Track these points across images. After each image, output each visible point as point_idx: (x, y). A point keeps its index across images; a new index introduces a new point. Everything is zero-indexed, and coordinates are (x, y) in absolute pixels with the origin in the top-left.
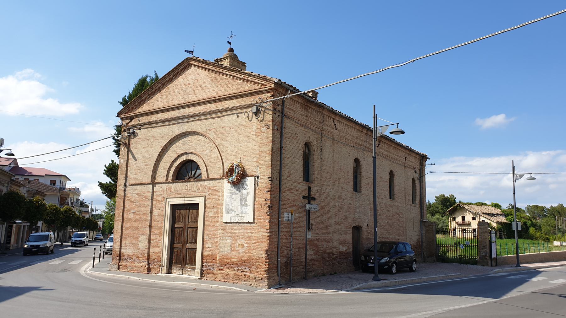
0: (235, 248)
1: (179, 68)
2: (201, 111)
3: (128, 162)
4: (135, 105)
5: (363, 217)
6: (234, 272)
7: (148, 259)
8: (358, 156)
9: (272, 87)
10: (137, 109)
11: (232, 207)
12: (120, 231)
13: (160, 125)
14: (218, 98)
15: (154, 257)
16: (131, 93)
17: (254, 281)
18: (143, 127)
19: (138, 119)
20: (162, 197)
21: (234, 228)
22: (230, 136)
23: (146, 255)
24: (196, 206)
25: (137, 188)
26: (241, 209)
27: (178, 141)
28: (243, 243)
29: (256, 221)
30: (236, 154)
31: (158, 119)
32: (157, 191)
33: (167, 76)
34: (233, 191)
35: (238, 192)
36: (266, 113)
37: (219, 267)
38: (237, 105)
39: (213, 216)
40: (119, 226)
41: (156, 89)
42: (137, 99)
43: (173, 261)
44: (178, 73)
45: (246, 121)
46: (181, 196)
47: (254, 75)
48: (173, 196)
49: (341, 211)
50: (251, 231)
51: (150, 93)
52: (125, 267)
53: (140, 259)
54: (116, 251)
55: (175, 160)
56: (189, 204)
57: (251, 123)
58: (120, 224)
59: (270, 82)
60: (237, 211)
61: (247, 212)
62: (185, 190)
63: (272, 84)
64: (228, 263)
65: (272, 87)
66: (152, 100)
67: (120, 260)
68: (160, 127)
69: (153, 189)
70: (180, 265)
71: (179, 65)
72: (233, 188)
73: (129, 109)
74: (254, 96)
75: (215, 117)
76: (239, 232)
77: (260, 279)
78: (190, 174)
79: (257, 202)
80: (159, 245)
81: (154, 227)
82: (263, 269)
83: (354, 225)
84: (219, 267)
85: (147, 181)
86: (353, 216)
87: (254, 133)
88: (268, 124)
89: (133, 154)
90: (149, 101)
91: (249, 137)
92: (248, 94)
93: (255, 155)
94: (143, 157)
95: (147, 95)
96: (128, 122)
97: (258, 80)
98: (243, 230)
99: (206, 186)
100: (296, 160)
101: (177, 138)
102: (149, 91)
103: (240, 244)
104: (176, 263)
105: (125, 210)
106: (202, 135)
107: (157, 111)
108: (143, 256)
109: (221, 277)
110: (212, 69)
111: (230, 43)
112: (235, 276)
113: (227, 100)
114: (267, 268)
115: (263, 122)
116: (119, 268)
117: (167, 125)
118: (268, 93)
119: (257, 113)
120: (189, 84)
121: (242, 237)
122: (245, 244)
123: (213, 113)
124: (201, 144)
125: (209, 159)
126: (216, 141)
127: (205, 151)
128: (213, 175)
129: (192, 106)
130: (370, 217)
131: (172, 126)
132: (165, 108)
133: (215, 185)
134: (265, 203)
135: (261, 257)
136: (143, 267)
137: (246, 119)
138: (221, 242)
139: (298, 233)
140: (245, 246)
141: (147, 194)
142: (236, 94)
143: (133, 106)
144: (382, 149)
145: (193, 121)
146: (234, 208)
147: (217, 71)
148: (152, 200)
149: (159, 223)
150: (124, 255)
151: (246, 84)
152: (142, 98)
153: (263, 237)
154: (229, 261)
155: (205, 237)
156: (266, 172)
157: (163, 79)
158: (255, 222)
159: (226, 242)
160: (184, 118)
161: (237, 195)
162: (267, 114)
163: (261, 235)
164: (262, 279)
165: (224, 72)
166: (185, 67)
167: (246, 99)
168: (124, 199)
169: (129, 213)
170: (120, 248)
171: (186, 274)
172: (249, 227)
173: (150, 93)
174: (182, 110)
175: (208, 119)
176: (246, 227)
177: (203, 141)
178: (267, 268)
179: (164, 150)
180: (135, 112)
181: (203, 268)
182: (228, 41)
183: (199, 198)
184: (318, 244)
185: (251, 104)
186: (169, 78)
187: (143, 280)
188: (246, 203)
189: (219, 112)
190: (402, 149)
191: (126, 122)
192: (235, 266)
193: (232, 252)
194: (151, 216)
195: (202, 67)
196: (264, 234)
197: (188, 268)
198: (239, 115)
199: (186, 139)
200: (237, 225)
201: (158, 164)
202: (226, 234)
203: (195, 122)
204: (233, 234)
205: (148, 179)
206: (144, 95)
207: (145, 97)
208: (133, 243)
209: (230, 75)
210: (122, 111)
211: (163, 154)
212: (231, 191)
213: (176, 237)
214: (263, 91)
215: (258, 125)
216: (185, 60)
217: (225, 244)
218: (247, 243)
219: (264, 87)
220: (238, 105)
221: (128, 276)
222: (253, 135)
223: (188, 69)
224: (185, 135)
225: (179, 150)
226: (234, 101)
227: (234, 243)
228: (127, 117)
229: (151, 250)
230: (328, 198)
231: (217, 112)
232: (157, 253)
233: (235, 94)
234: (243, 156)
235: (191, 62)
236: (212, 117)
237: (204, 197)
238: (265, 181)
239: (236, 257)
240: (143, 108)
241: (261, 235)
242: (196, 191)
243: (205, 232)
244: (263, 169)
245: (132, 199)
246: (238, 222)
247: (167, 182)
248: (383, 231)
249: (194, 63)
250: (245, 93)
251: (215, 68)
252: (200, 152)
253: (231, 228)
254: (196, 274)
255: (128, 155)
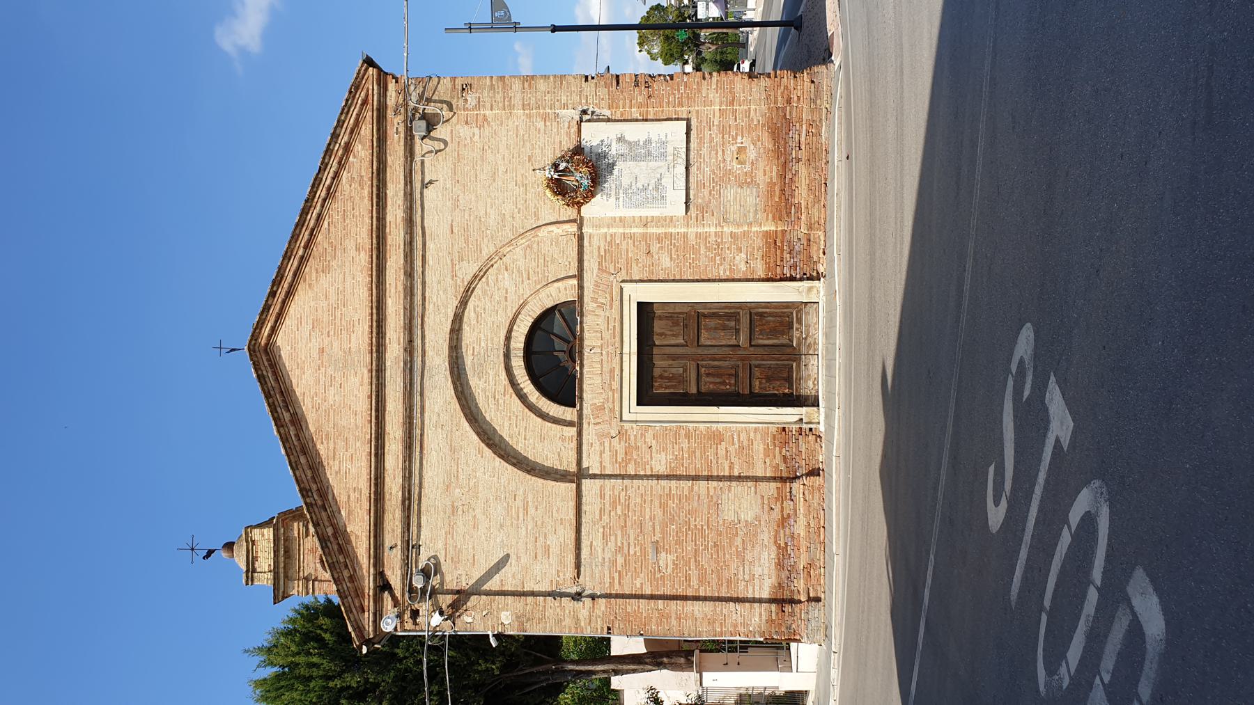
0: (746, 173)
1: (270, 385)
2: (402, 302)
3: (511, 591)
4: (343, 568)
6: (803, 170)
7: (783, 480)
9: (375, 73)
10: (358, 563)
11: (651, 188)
12: (708, 607)
13: (418, 461)
14: (374, 241)
15: (778, 460)
17: (818, 101)
18: (415, 537)
19: (387, 549)
20: (617, 437)
21: (701, 181)
22: (477, 208)
23: (773, 485)
24: (645, 310)
25: (589, 543)
26: (655, 159)
27: (471, 394)
28: (734, 148)
29: (684, 116)
30: (523, 186)
31: (400, 466)
32: (601, 462)
33: (282, 431)
34: (613, 186)
35: (615, 172)
36: (433, 95)
37: (793, 220)
38: (402, 182)
39: (671, 255)
40: (696, 612)
41: (313, 477)
42: (330, 554)
43: (784, 394)
44: (282, 392)
45: (446, 158)
46: (617, 372)
47: (338, 121)
48: (617, 396)
50: (707, 129)
51: (320, 503)
52: (812, 572)
53: (785, 516)
54: (767, 621)
55: (522, 397)
56: (637, 338)
57: (452, 142)
58: (690, 606)
59: (363, 78)
60: (660, 171)
61: (664, 139)
62: (604, 353)
63: (367, 74)
64: (783, 190)
65: (375, 73)
66: (341, 498)
67: (792, 601)
68: (424, 462)
69: (594, 476)
70: (794, 364)
71: (263, 382)
72: (605, 185)
73: (352, 594)
74: (388, 132)
75: (424, 257)
76: (710, 162)
77: (813, 85)
78: (560, 355)
79: (640, 116)
80: (745, 443)
81: (698, 467)
82: (792, 81)
84: (793, 220)
85: (571, 503)
87: (476, 130)
88: (460, 88)
89: (489, 575)
90: (343, 512)
91: (486, 147)
92: (379, 146)
93: (530, 127)
94: (501, 526)
95: (324, 514)
96: (390, 599)
97: (351, 113)
98: (704, 151)
99: (597, 285)
101: (461, 392)
102: (311, 504)
103: (737, 158)
104: (789, 380)
105: (648, 592)
106: (464, 303)
107: (376, 468)
108: (777, 499)
109: (816, 206)
110: (296, 263)
111: (210, 553)
112: (812, 163)
113: (386, 214)
114: (789, 72)
115: (454, 102)
116: (818, 600)
117: (422, 435)
118: (386, 89)
119: (431, 123)
120: (322, 351)
121: (720, 153)
122: (736, 143)
123: (411, 265)
124: (487, 307)
125: (529, 279)
126: (484, 252)
127: (507, 290)
128: (570, 263)
129: (384, 337)
131: (426, 415)
132: (373, 436)
133: (596, 253)
134: (643, 88)
135: (766, 90)
136: (806, 493)
137: (440, 158)
138: (732, 220)
140: (742, 143)
141: (607, 497)
142: (375, 182)
143: (346, 573)
145: (423, 337)
146: (653, 181)
147: (306, 247)
148: (623, 477)
149: (685, 445)
150: (779, 584)
151: (355, 157)
152: (330, 534)
153: (721, 88)
154: (777, 189)
155: (722, 275)
156: (573, 89)
157: (287, 445)
158: (686, 117)
159: (732, 204)
160: (411, 366)
161: (624, 173)
162: (436, 93)
163: (717, 93)
164: (813, 82)
165: (312, 224)
166: (271, 365)
167: (390, 155)
168: (617, 596)
169: (658, 575)
170: (760, 601)
171: (815, 343)
172: (697, 133)
173: (320, 503)
174: (388, 374)
175: (424, 283)
176: (698, 143)
177: (480, 299)
178: (789, 72)
179: (491, 442)
180: (366, 574)
181: (798, 276)
182: (204, 558)
183: (624, 302)
185: (406, 138)
186: (289, 424)
187: (839, 394)
188: (641, 143)
189: (411, 242)
191: (389, 608)
192: (787, 170)
193: (756, 181)
194: (668, 477)
195: (284, 302)
196: (714, 86)
197: (799, 338)
198: (426, 182)
199: (468, 360)
200: (693, 170)
201: (527, 465)
202: (714, 203)
203: (426, 328)
204: (713, 183)
205: (568, 488)
206: (322, 525)
207: (327, 523)
208: (744, 549)
209: (322, 206)
210: (354, 623)
211: (500, 448)
212: (613, 193)
213: (723, 387)
214: (379, 101)
215: (458, 121)
216: (252, 360)
217: (738, 206)
218: (735, 139)
219: (370, 101)
220: (402, 177)
221: (834, 458)
222: (480, 136)
223: (280, 356)
224: (457, 363)
225: (495, 385)
226: (390, 192)
227: (736, 177)
228: (375, 602)
229: (760, 473)
231: (411, 251)
232: (765, 449)
233: (374, 185)
234: (529, 162)
235: (263, 342)
236: (420, 270)
237: (623, 285)
238: (594, 89)
239: (768, 168)
240: (357, 537)
241: (717, 93)
242: (607, 314)
243: (710, 276)
244: (565, 98)
245: (620, 560)
246: (687, 168)
247: (579, 425)
249: (266, 331)
250: (375, 154)
251: (294, 253)
252: (509, 308)
253: (701, 189)
254: (815, 292)
255: (488, 593)
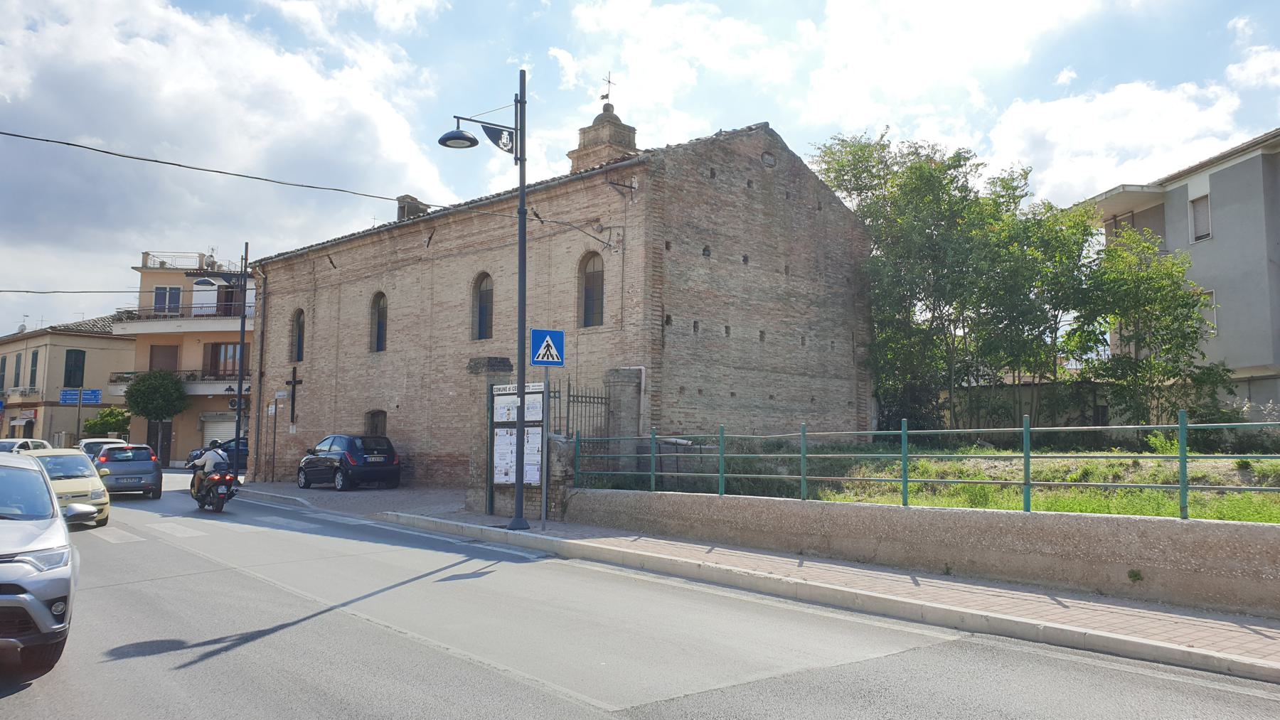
5: (386, 394)
8: (380, 287)
16: (1216, 395)
49: (343, 390)
83: (367, 410)
86: (366, 394)
100: (282, 339)
130: (405, 391)
139: (281, 428)
144: (441, 242)
184: (306, 441)
190: (510, 205)
230: (323, 375)
248: (443, 414)
